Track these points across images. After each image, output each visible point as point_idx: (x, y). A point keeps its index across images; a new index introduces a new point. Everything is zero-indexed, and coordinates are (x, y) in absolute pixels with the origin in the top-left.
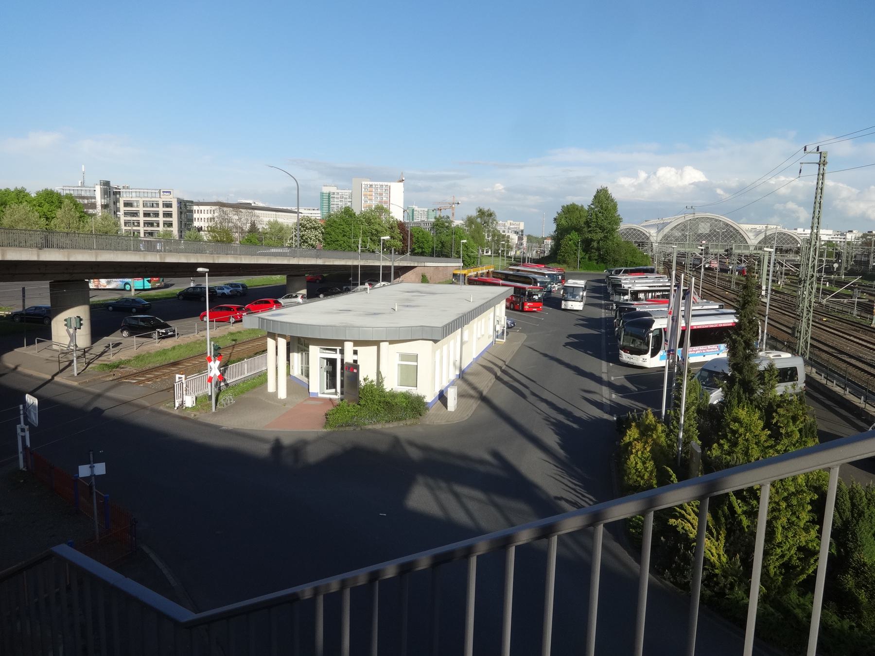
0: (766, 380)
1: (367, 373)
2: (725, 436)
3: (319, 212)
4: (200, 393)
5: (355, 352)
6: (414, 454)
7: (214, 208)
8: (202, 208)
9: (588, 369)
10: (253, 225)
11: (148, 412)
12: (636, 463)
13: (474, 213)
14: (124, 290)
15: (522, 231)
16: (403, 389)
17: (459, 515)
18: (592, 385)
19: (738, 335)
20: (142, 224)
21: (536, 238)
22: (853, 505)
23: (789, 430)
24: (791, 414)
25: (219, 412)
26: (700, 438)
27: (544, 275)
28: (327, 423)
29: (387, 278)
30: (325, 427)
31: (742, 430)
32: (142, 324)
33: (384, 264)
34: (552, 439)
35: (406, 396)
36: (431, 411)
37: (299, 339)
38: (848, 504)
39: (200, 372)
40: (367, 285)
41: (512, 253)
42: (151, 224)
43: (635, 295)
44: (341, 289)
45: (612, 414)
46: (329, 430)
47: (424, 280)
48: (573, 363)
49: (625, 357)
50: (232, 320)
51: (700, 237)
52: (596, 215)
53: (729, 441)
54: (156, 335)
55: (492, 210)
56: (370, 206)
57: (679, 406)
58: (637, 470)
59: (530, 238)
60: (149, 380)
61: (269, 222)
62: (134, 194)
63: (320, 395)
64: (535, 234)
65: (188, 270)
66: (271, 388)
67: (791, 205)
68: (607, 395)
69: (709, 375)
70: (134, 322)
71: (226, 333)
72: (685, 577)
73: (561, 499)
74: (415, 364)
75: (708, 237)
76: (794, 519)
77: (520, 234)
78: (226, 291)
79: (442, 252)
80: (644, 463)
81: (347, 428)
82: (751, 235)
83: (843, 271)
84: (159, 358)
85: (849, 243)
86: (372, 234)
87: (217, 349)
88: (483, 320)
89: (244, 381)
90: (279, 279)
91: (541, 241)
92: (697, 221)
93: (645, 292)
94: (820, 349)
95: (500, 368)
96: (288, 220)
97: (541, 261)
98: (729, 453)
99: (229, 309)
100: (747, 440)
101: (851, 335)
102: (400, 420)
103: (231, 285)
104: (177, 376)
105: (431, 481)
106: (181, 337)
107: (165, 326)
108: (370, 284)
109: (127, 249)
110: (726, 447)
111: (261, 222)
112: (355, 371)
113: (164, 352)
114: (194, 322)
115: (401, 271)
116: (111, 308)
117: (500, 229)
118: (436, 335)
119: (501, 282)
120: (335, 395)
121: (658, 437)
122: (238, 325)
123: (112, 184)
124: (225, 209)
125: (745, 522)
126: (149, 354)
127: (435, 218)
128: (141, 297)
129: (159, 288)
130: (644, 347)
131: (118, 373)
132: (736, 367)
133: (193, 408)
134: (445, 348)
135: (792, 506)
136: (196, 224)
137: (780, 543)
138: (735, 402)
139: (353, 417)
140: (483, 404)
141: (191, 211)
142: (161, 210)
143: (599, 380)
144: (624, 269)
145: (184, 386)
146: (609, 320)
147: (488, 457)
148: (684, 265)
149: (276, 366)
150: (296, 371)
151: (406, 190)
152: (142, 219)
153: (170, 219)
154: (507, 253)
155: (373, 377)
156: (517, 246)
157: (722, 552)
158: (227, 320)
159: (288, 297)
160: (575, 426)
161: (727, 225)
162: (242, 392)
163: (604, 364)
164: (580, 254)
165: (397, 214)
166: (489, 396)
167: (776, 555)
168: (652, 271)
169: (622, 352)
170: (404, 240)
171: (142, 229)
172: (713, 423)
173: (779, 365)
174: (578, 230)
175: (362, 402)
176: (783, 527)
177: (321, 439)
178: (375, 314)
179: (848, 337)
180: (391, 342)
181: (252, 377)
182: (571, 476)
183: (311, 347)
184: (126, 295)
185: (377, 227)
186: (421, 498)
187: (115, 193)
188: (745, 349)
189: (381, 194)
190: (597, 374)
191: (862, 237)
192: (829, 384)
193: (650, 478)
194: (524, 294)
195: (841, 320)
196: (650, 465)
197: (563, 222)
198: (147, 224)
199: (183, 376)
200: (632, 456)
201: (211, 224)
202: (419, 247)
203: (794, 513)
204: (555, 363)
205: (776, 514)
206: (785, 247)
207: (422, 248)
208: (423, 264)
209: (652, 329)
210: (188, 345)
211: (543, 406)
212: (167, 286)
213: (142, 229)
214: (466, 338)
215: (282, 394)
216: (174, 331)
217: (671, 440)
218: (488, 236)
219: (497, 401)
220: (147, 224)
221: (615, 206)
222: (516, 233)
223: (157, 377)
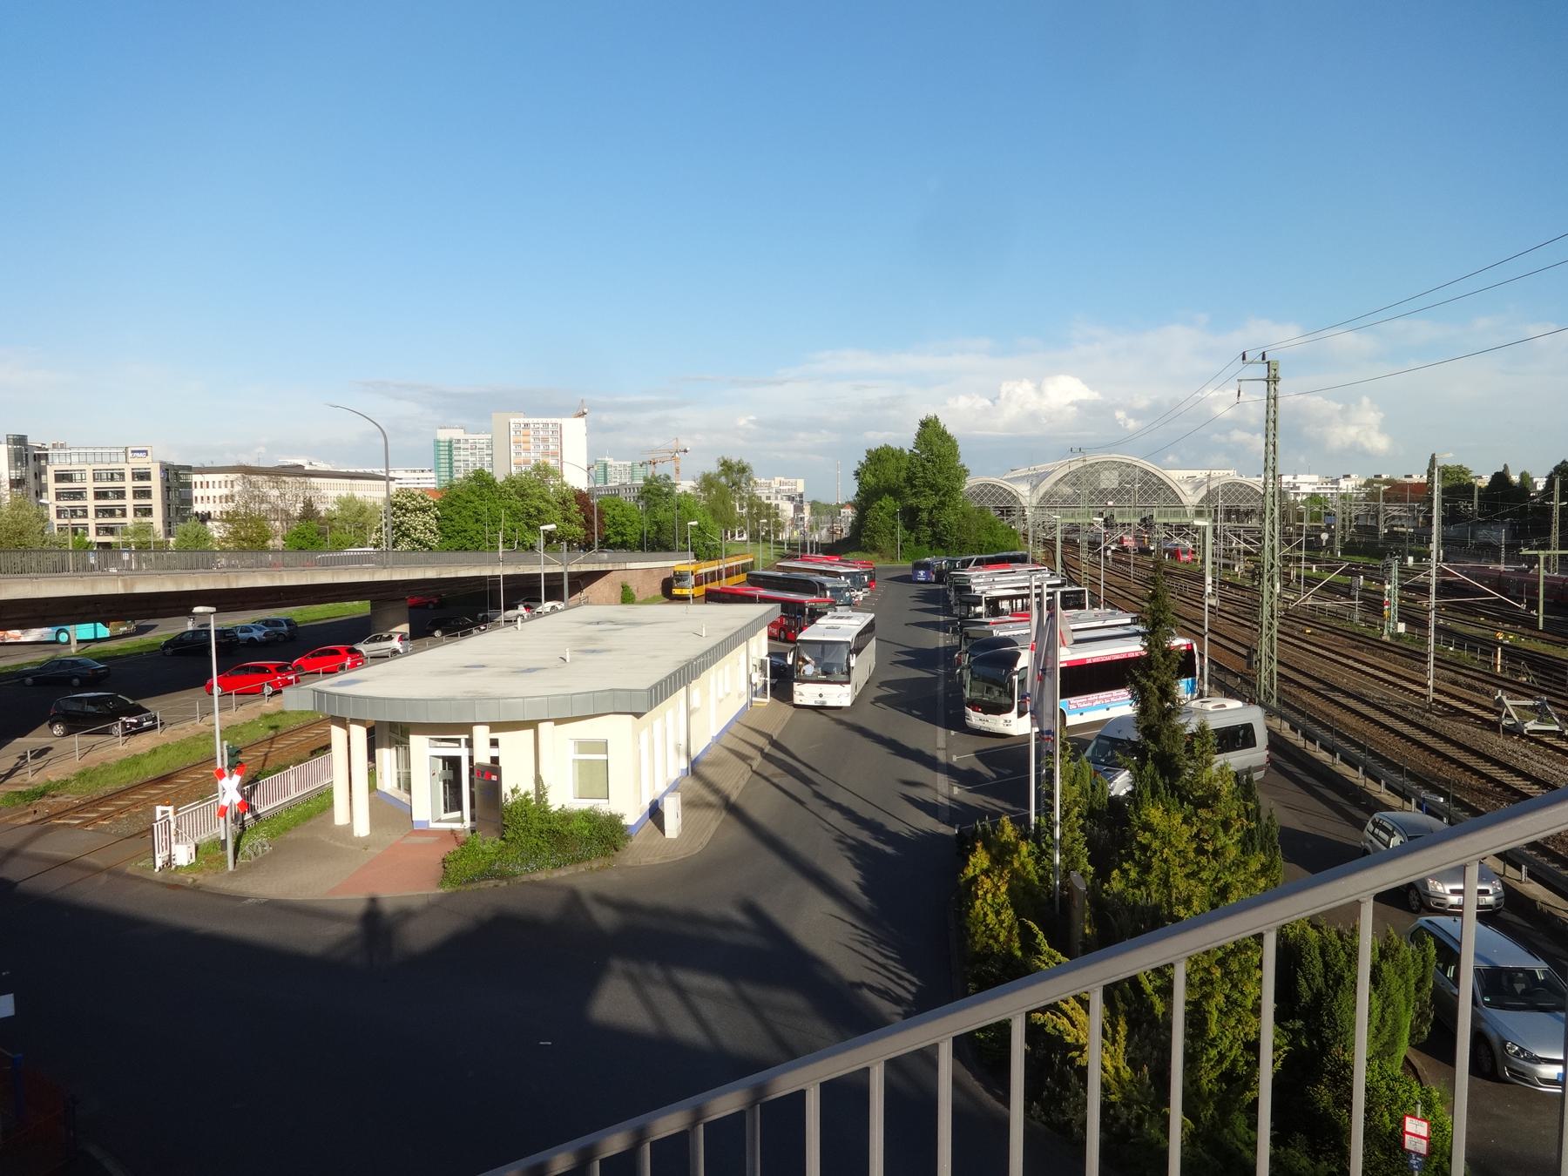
0: (1197, 753)
1: (516, 780)
2: (1130, 856)
3: (432, 475)
4: (204, 837)
5: (494, 743)
6: (605, 918)
7: (232, 477)
8: (209, 477)
9: (912, 744)
10: (308, 505)
11: (104, 878)
12: (985, 915)
13: (713, 468)
14: (57, 642)
15: (801, 495)
16: (584, 805)
17: (685, 1028)
18: (919, 772)
19: (1149, 677)
20: (91, 513)
21: (827, 506)
22: (1326, 965)
23: (1219, 845)
24: (1220, 817)
25: (240, 870)
26: (1091, 862)
27: (838, 575)
28: (446, 877)
29: (554, 593)
30: (441, 884)
31: (1156, 844)
32: (91, 709)
33: (550, 570)
34: (847, 875)
35: (590, 817)
36: (635, 842)
37: (393, 726)
38: (1319, 964)
39: (202, 797)
40: (521, 610)
41: (784, 536)
42: (110, 512)
43: (993, 604)
44: (474, 618)
45: (951, 824)
46: (448, 889)
47: (627, 597)
48: (887, 734)
49: (975, 718)
50: (268, 690)
51: (1104, 494)
52: (923, 466)
53: (1137, 863)
54: (118, 729)
55: (746, 461)
56: (527, 462)
57: (1052, 809)
58: (987, 926)
59: (815, 506)
60: (104, 817)
61: (339, 497)
62: (75, 459)
63: (433, 825)
64: (824, 500)
65: (180, 603)
66: (340, 818)
67: (1238, 436)
68: (945, 790)
69: (1107, 747)
70: (75, 707)
71: (256, 716)
72: (1063, 1113)
73: (861, 985)
74: (604, 757)
75: (1117, 493)
76: (1236, 995)
77: (797, 501)
78: (257, 634)
79: (656, 543)
80: (998, 913)
81: (483, 885)
82: (1187, 488)
83: (1338, 546)
84: (126, 773)
85: (1344, 497)
86: (529, 515)
87: (234, 753)
88: (727, 668)
89: (289, 808)
90: (360, 608)
91: (833, 511)
92: (1094, 469)
93: (1010, 598)
94: (1300, 685)
95: (761, 750)
96: (372, 494)
97: (833, 549)
98: (1138, 885)
99: (261, 670)
100: (1165, 861)
101: (1348, 658)
102: (579, 861)
103: (266, 623)
104: (159, 809)
105: (635, 968)
106: (169, 729)
107: (139, 710)
108: (527, 608)
109: (59, 569)
110: (1133, 875)
111: (323, 499)
112: (494, 778)
113: (136, 760)
114: (193, 696)
115: (581, 581)
116: (29, 680)
117: (762, 493)
118: (639, 704)
119: (763, 592)
120: (462, 822)
121: (1022, 864)
122: (276, 699)
123: (31, 441)
124: (254, 478)
125: (1159, 1008)
126: (106, 768)
127: (645, 479)
128: (90, 655)
129: (125, 635)
130: (1005, 700)
131: (45, 806)
132: (1150, 732)
133: (191, 866)
134: (657, 724)
135: (1231, 973)
136: (198, 508)
137: (1214, 1039)
138: (1147, 794)
139: (492, 863)
140: (731, 819)
141: (188, 485)
142: (129, 485)
143: (931, 763)
144: (975, 557)
145: (173, 826)
146: (949, 651)
147: (739, 917)
148: (1067, 551)
149: (349, 778)
150: (388, 782)
151: (591, 430)
152: (91, 503)
153: (147, 502)
154: (776, 536)
155: (527, 786)
156: (792, 523)
157: (1121, 1063)
158: (258, 691)
159: (374, 640)
160: (889, 850)
161: (1147, 473)
162: (286, 829)
163: (941, 732)
164: (900, 532)
165: (576, 478)
166: (742, 803)
167: (1209, 1060)
168: (1022, 560)
169: (969, 711)
170: (588, 523)
171: (92, 522)
172: (1111, 829)
173: (1215, 723)
174: (895, 492)
175: (509, 835)
176: (1220, 1011)
177: (433, 906)
178: (529, 670)
179: (1345, 661)
180: (558, 722)
181: (306, 799)
182: (880, 942)
183: (412, 738)
184: (63, 653)
185: (536, 503)
186: (618, 1002)
187: (37, 458)
188: (1160, 700)
189: (545, 440)
190: (928, 752)
191: (1366, 485)
192: (1310, 746)
193: (1009, 939)
194: (803, 613)
195: (1333, 630)
196: (1008, 915)
197: (869, 478)
198: (101, 512)
199: (170, 809)
200: (978, 903)
201: (230, 507)
202: (617, 533)
203: (1234, 986)
204: (857, 737)
205: (1207, 989)
206: (1243, 506)
207: (623, 535)
208: (622, 566)
209: (1017, 669)
210: (182, 744)
211: (835, 817)
212: (141, 630)
213: (92, 522)
214: (696, 702)
215: (362, 828)
216: (155, 719)
217: (1043, 868)
218: (742, 507)
219: (756, 811)
220: (101, 512)
221: (954, 446)
222: (791, 499)
223: (120, 810)
